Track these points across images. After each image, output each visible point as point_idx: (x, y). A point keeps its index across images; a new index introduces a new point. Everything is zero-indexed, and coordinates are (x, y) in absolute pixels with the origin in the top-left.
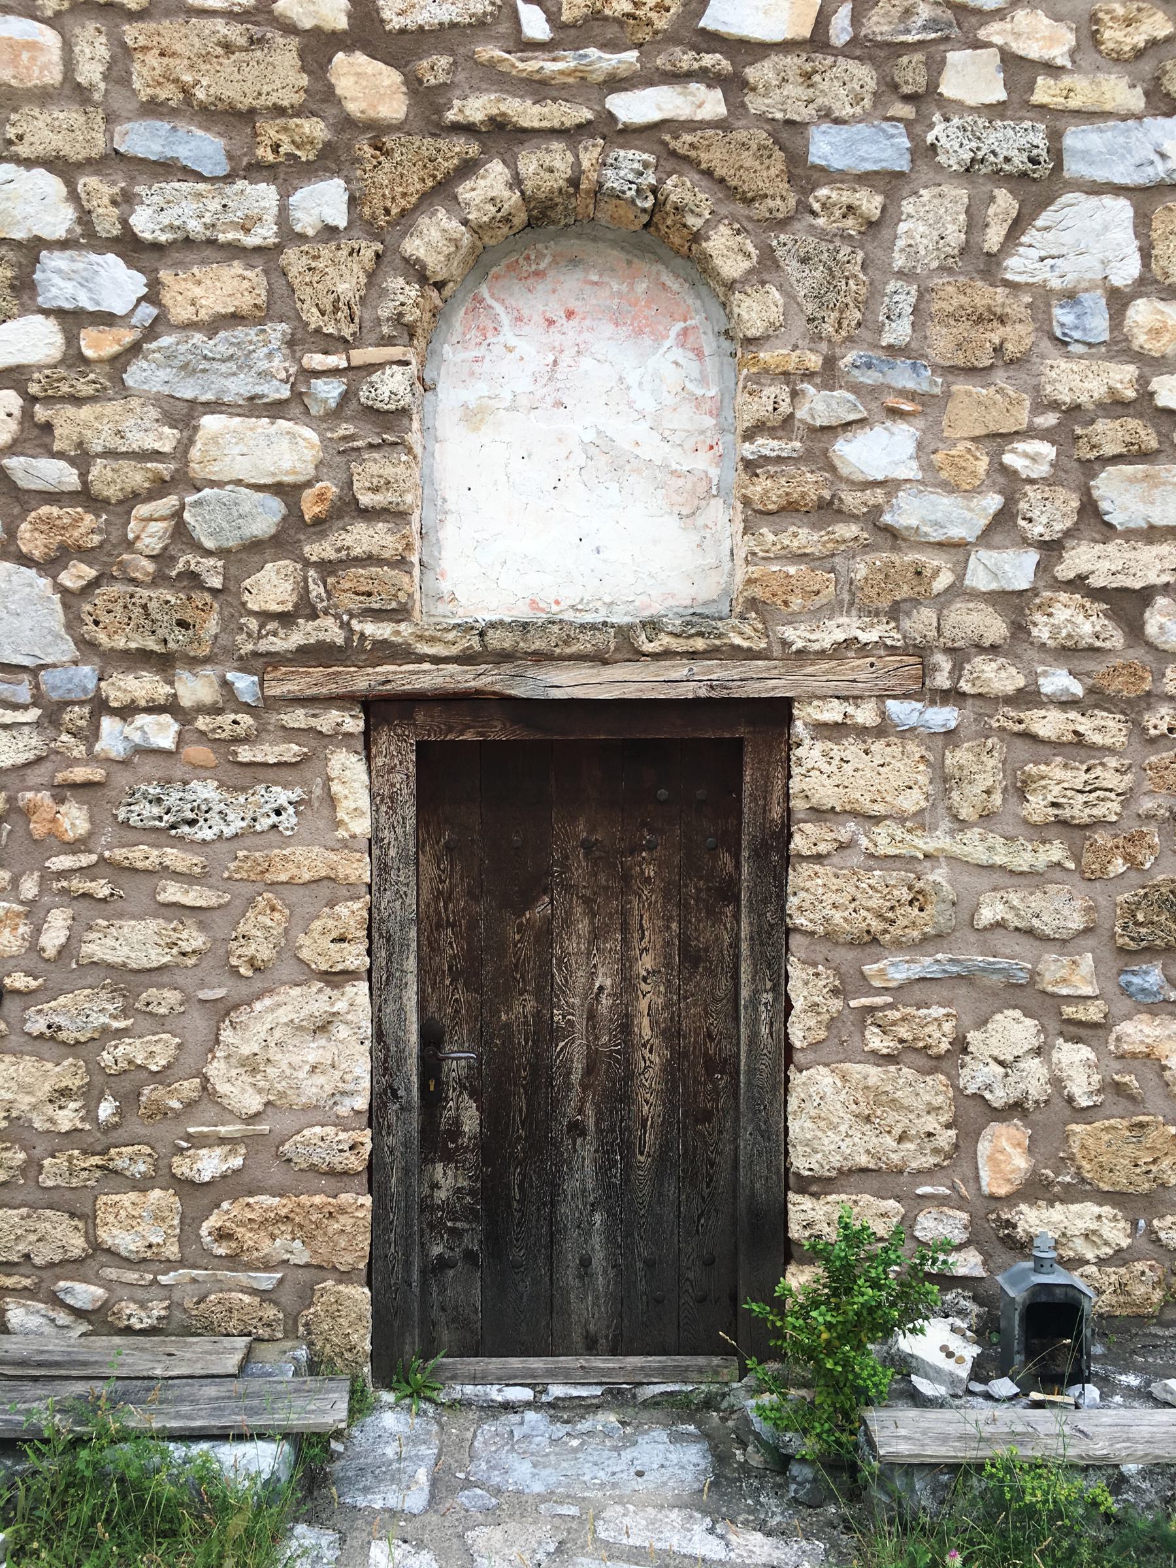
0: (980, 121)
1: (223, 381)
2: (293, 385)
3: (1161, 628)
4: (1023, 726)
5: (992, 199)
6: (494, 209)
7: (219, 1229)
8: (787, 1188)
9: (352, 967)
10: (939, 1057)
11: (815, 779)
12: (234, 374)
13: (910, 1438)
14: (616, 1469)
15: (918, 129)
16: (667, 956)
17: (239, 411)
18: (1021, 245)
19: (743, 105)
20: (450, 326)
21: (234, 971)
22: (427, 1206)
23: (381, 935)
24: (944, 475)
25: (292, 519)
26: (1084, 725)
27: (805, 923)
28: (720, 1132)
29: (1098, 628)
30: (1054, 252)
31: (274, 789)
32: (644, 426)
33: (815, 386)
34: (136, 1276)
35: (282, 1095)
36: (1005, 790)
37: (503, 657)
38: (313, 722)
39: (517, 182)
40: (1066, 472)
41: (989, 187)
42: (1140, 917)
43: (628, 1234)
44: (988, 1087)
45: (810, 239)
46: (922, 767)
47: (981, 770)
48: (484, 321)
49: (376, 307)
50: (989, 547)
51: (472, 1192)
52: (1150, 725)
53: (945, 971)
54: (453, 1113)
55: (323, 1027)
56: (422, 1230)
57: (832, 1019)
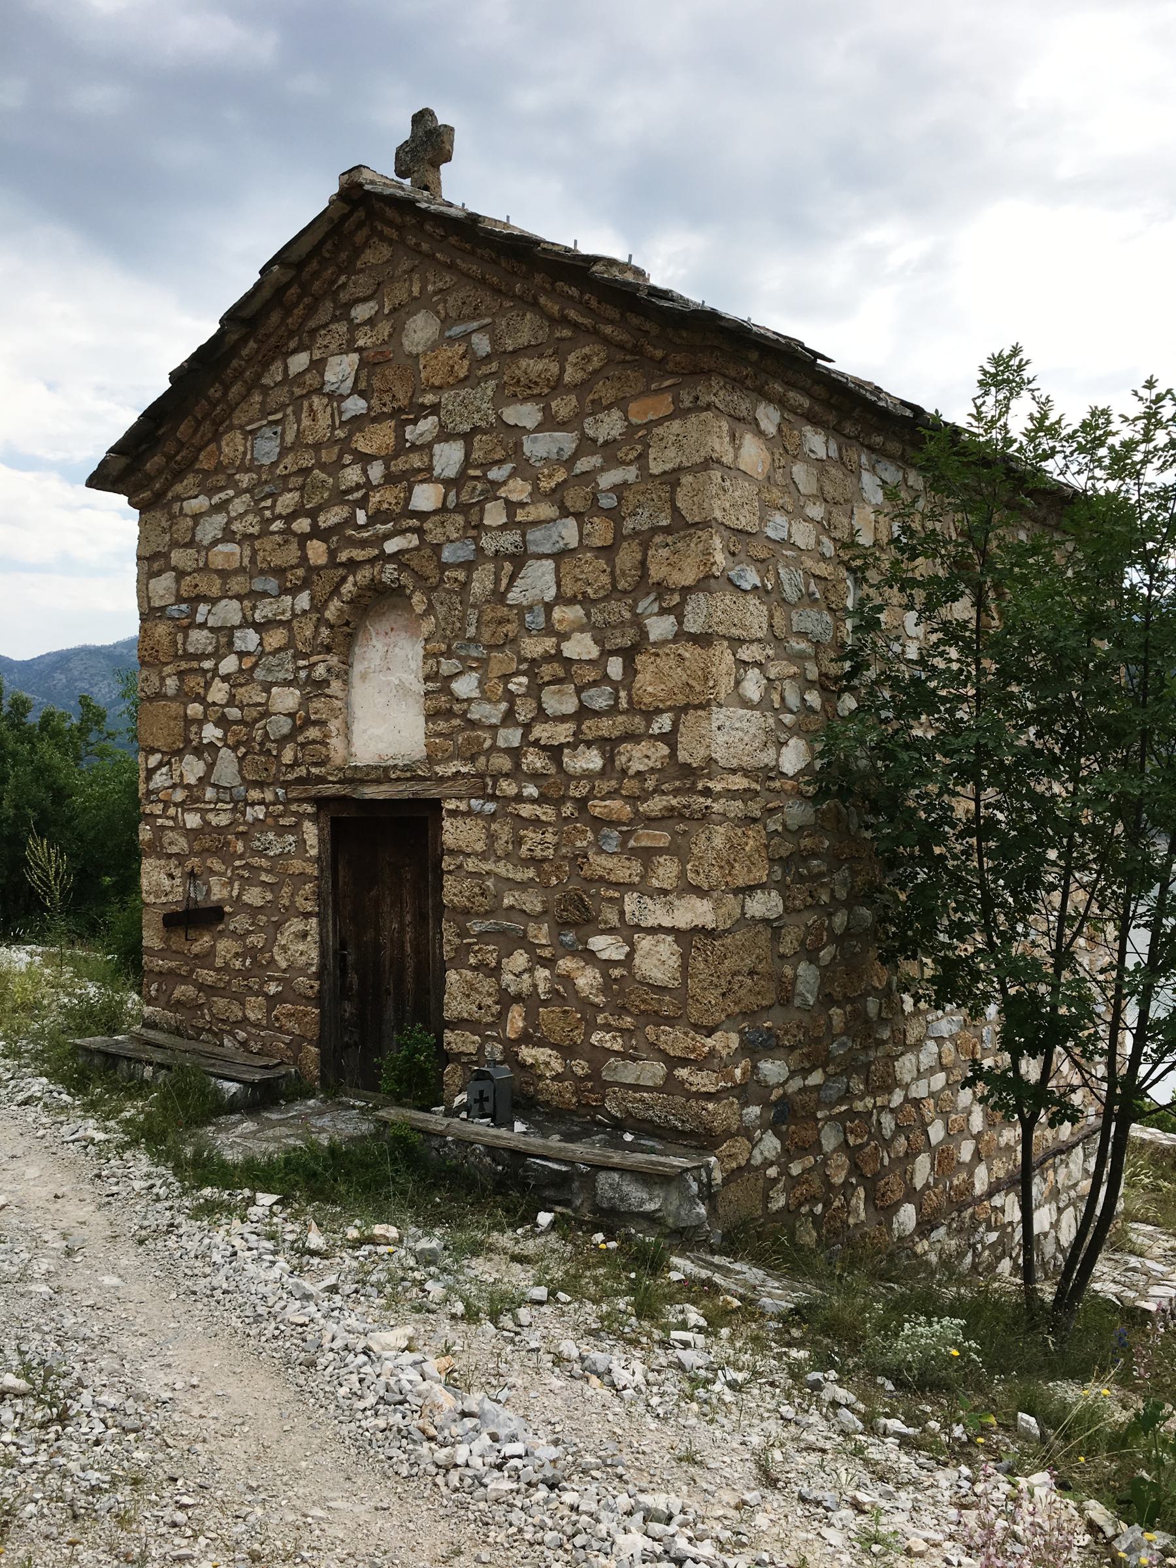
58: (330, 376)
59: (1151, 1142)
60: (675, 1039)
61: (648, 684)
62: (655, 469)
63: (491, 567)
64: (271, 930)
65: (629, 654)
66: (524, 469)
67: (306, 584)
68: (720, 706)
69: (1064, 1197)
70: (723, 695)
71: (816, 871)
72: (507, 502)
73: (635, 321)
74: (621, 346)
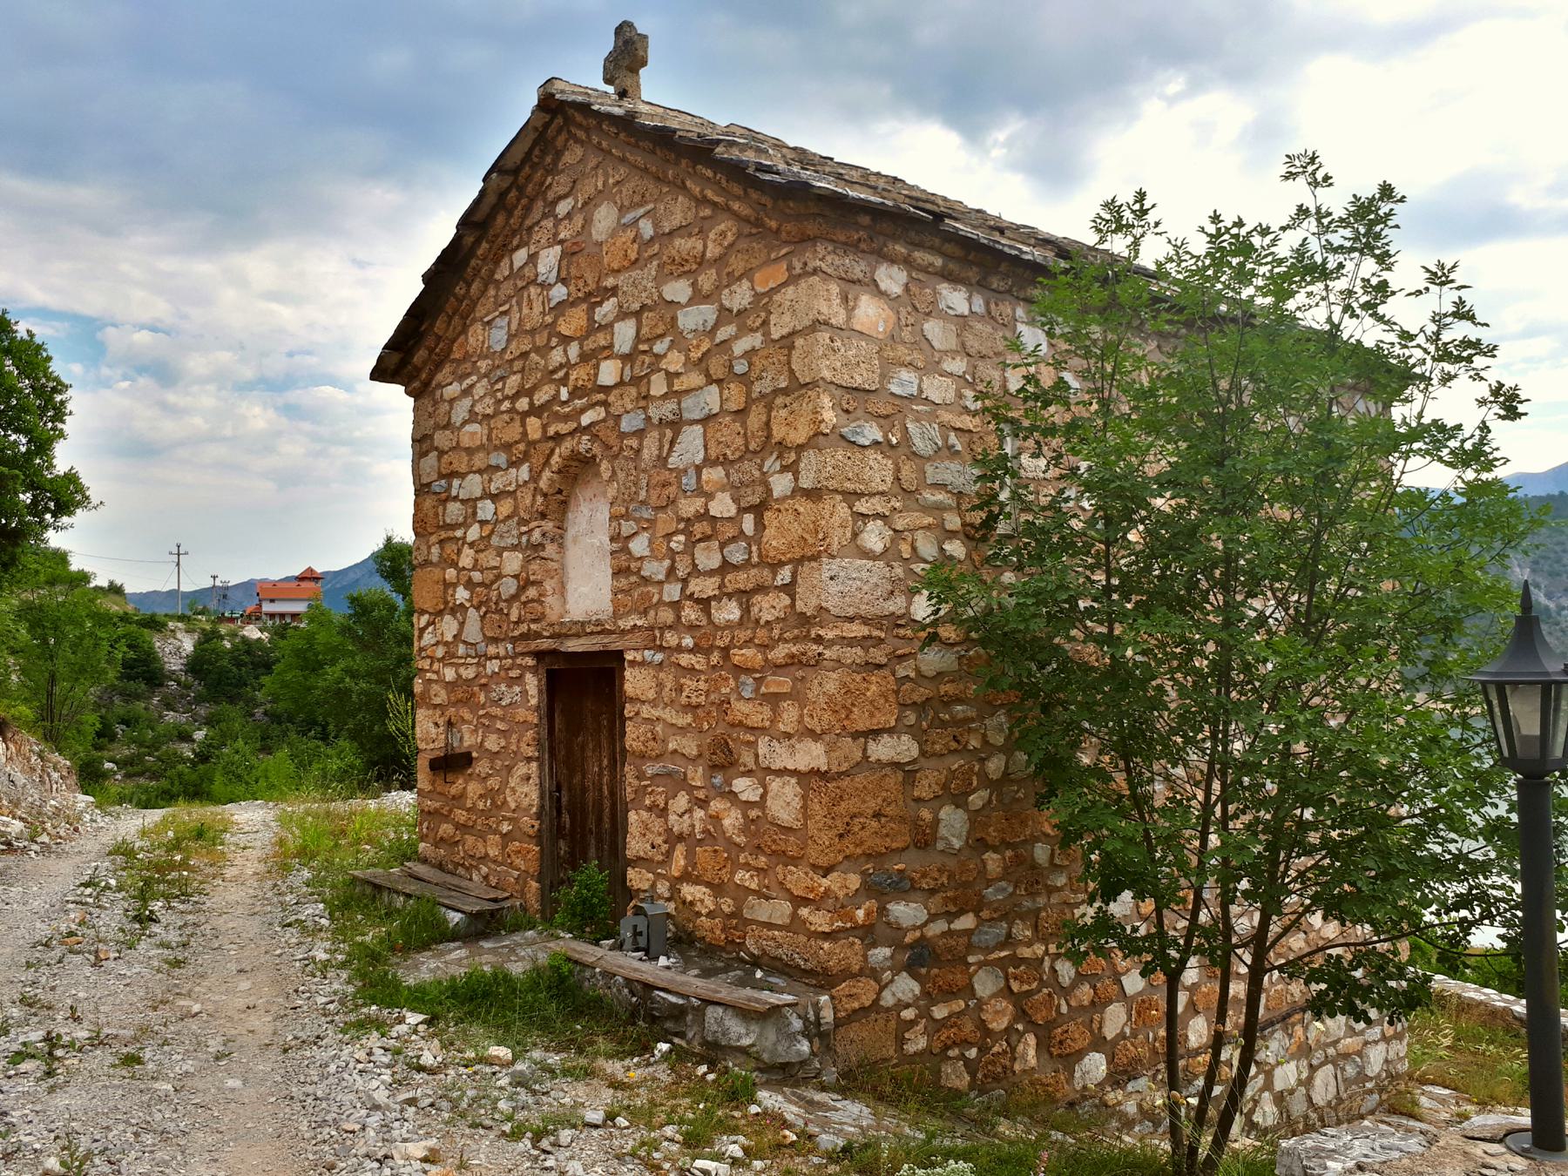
58: (541, 269)
59: (1480, 1003)
60: (798, 879)
61: (774, 540)
62: (775, 336)
63: (655, 434)
64: (504, 773)
65: (759, 510)
66: (679, 341)
67: (526, 456)
68: (833, 557)
69: (1319, 1055)
70: (835, 546)
71: (961, 716)
72: (668, 373)
73: (754, 195)
74: (747, 220)
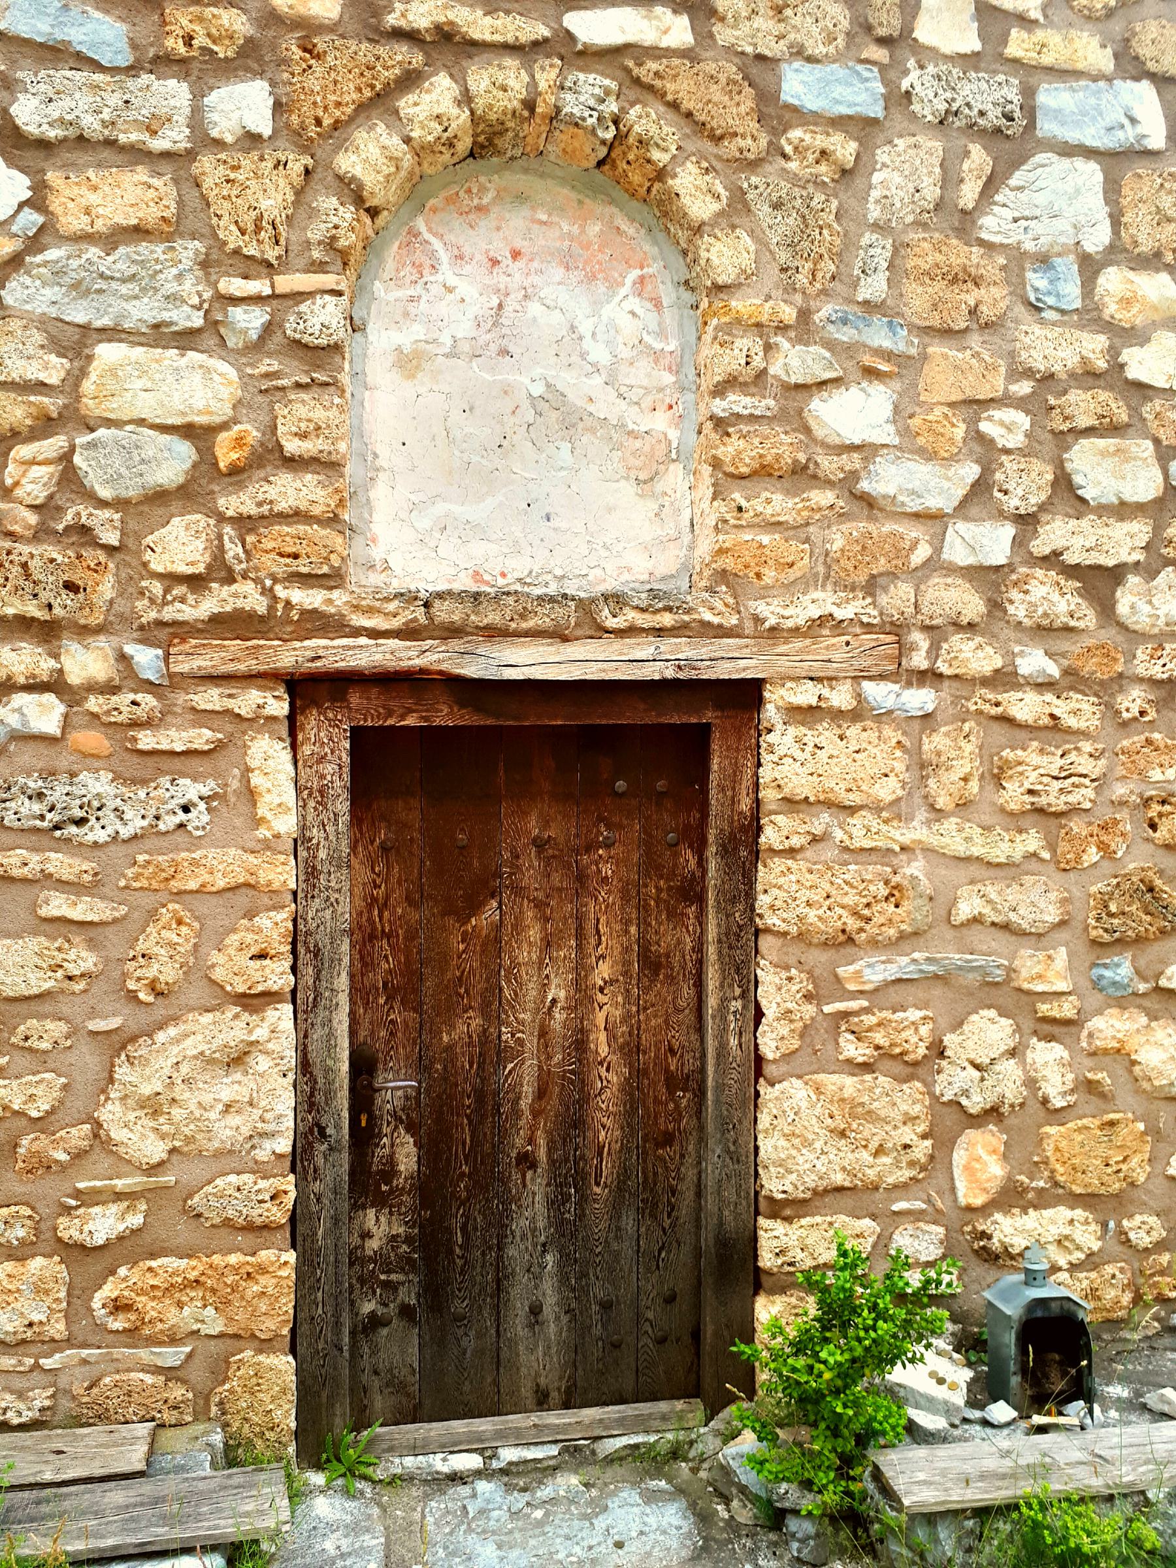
0: (955, 71)
1: (124, 304)
2: (207, 312)
3: (1132, 607)
4: (1000, 710)
5: (967, 153)
6: (440, 129)
7: (116, 1300)
8: (757, 1213)
9: (275, 988)
10: (916, 1064)
11: (788, 767)
12: (136, 297)
13: (931, 1483)
14: (594, 1543)
15: (892, 75)
16: (627, 963)
17: (143, 339)
18: (995, 203)
19: (711, 36)
20: (381, 261)
21: (132, 996)
22: (356, 1258)
23: (308, 950)
24: (921, 441)
25: (204, 468)
26: (1061, 708)
27: (778, 922)
28: (682, 1156)
29: (1073, 607)
30: (1027, 213)
31: (181, 781)
32: (598, 380)
33: (790, 340)
34: (13, 1361)
35: (189, 1140)
36: (982, 777)
37: (452, 632)
38: (230, 704)
39: (466, 98)
40: (1040, 443)
41: (963, 141)
42: (1113, 908)
43: (584, 1275)
44: (966, 1093)
45: (783, 183)
46: (898, 753)
47: (959, 754)
48: (419, 257)
49: (305, 229)
50: (966, 519)
51: (408, 1240)
52: (1123, 707)
53: (921, 971)
54: (387, 1151)
55: (237, 1059)
56: (351, 1286)
57: (805, 1026)
63: (934, 145)
